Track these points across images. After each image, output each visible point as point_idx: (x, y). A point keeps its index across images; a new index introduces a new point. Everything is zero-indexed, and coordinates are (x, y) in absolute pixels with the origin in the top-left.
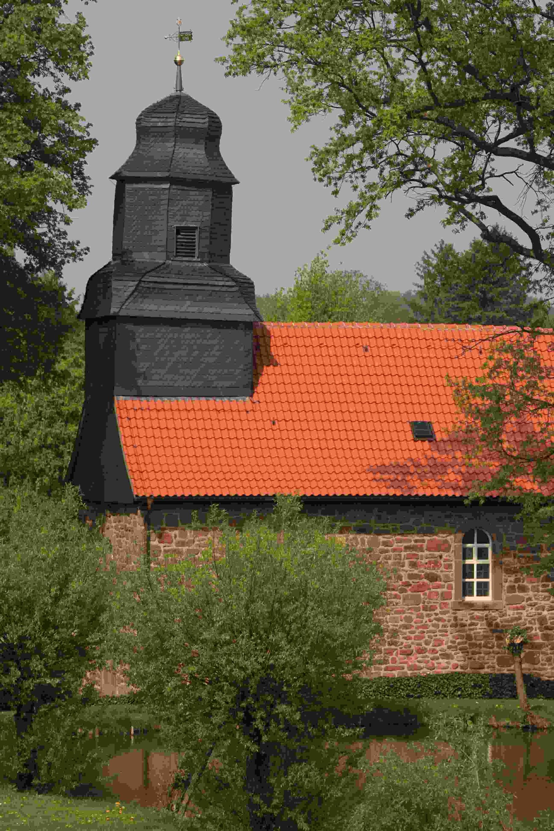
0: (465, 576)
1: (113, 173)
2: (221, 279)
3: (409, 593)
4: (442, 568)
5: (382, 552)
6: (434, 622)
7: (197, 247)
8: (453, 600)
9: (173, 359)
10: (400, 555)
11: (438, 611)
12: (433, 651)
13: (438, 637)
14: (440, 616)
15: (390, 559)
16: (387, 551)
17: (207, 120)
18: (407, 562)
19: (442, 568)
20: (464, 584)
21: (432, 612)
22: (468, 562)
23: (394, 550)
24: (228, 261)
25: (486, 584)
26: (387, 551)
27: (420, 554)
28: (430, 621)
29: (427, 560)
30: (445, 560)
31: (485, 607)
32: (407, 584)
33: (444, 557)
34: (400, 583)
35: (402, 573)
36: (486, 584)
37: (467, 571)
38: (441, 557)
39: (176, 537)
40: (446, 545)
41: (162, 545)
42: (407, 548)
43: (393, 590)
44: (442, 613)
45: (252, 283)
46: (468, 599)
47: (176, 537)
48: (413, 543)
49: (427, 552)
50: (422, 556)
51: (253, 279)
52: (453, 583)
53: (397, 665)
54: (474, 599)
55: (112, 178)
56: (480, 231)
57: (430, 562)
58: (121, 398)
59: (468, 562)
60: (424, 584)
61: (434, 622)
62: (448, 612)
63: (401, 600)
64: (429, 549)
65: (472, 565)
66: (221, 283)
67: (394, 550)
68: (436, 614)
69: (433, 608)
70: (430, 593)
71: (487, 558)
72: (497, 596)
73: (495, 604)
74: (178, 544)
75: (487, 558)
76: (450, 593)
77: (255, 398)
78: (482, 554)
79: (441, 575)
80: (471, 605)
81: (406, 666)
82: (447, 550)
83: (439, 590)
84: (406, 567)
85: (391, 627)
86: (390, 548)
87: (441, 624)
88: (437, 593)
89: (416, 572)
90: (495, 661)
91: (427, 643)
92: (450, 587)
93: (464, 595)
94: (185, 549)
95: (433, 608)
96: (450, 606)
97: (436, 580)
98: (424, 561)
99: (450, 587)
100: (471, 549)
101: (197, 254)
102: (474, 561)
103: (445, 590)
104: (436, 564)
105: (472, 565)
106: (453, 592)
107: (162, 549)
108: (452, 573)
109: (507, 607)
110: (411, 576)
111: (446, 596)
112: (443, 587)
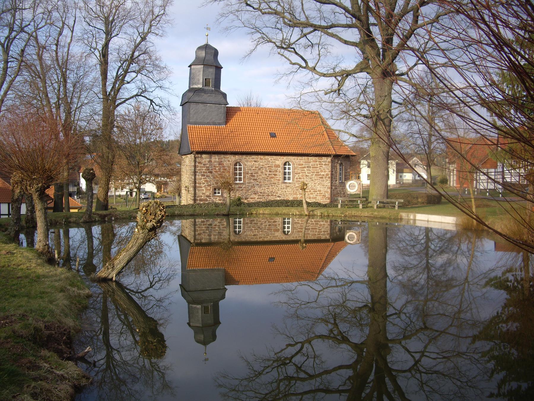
72: (293, 180)
80: (286, 183)
102: (287, 171)
104: (276, 171)
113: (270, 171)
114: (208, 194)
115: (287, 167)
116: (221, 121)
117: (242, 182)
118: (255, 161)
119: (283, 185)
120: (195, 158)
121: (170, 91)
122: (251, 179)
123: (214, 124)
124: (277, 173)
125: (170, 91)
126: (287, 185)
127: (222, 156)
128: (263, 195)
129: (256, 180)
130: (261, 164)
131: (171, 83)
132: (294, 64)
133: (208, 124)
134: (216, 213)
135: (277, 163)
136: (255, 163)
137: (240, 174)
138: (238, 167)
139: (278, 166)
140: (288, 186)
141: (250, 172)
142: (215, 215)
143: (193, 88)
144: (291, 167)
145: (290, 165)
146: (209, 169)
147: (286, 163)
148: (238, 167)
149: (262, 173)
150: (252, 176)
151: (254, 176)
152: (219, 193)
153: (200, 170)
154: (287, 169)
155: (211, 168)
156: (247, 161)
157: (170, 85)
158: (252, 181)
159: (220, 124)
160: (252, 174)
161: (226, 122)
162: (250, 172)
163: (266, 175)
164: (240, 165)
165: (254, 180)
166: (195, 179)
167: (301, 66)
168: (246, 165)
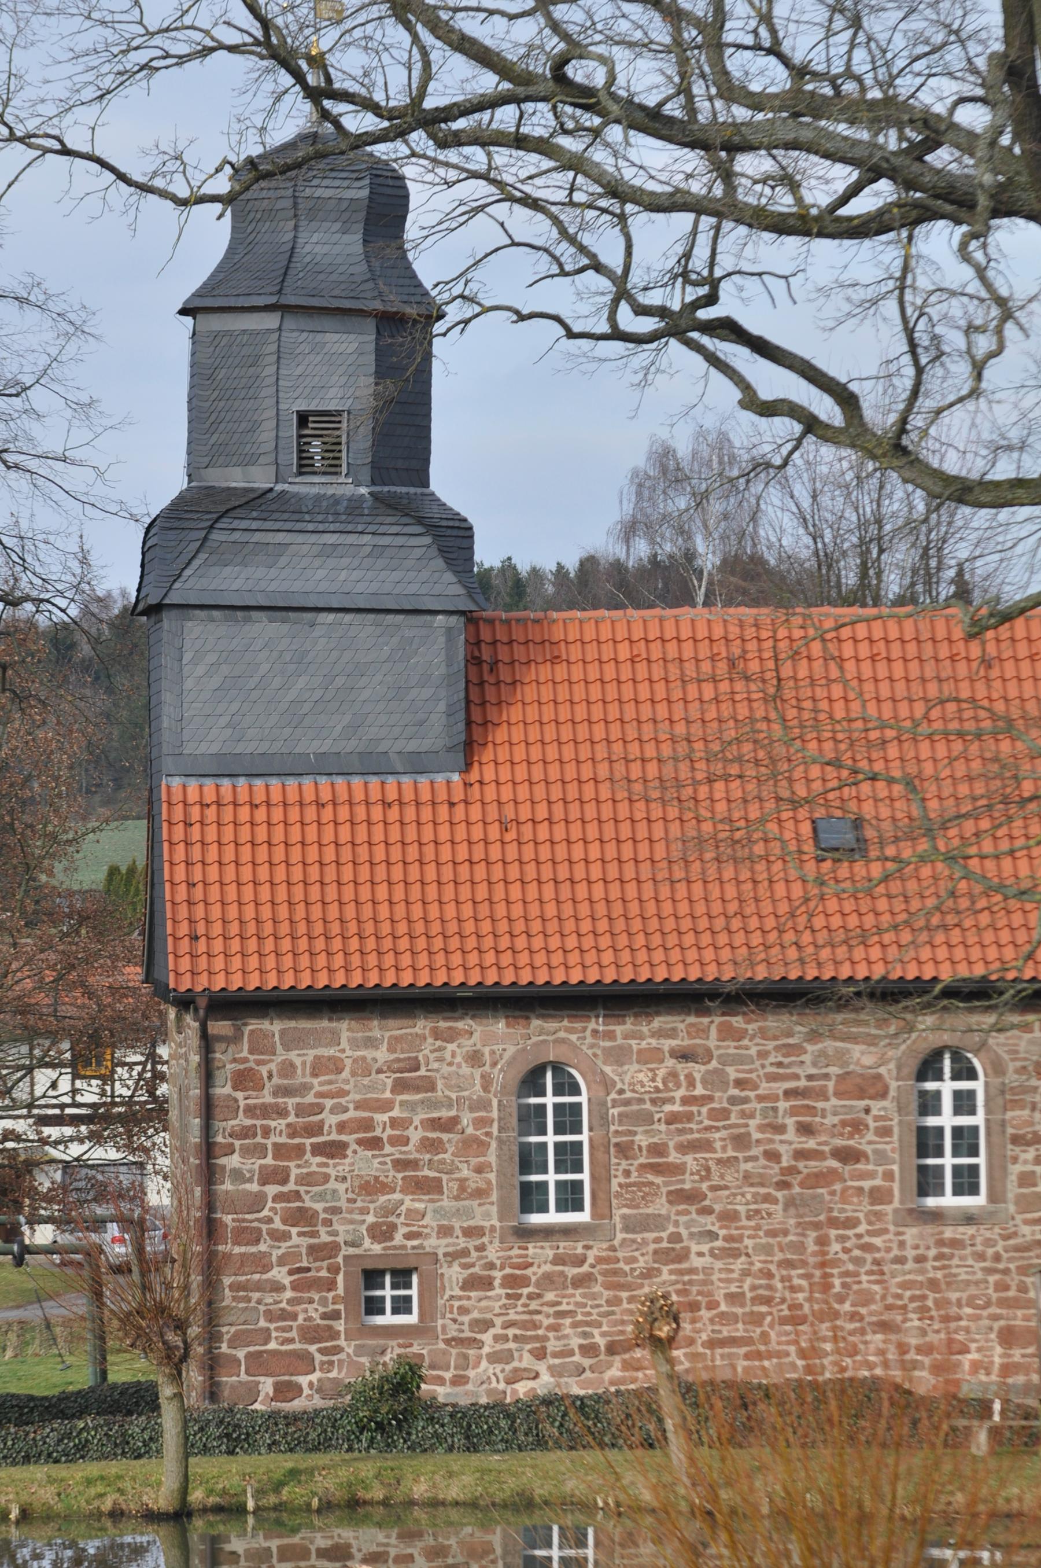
0: (923, 1150)
1: (180, 306)
2: (389, 520)
3: (797, 1190)
4: (870, 1136)
5: (733, 1101)
6: (857, 1253)
7: (344, 454)
8: (896, 1204)
9: (292, 695)
10: (775, 1109)
11: (862, 1229)
12: (854, 1316)
13: (865, 1285)
14: (867, 1239)
15: (752, 1116)
16: (746, 1100)
17: (367, 181)
18: (790, 1122)
19: (870, 1136)
20: (922, 1169)
21: (850, 1233)
22: (932, 1121)
23: (761, 1098)
24: (424, 481)
25: (974, 1169)
26: (746, 1100)
27: (820, 1105)
28: (846, 1251)
29: (836, 1120)
30: (877, 1119)
31: (969, 1218)
32: (792, 1171)
33: (874, 1112)
34: (776, 1169)
35: (782, 1149)
36: (974, 1169)
37: (927, 1142)
38: (867, 1111)
39: (270, 1077)
40: (879, 1085)
41: (240, 1095)
42: (788, 1094)
43: (762, 1185)
44: (869, 1233)
45: (471, 528)
46: (931, 1202)
47: (270, 1077)
48: (803, 1083)
49: (834, 1101)
50: (823, 1110)
51: (471, 520)
52: (895, 1168)
53: (774, 1346)
54: (948, 1200)
55: (184, 312)
56: (738, 395)
57: (844, 1123)
58: (176, 782)
59: (932, 1121)
60: (833, 1171)
61: (857, 1253)
62: (886, 1231)
63: (779, 1207)
64: (838, 1095)
65: (940, 1130)
66: (395, 529)
67: (761, 1098)
68: (859, 1236)
69: (851, 1223)
70: (844, 1190)
71: (580, 1132)
72: (993, 1197)
73: (992, 1214)
74: (277, 1092)
75: (580, 1132)
76: (890, 1191)
77: (474, 776)
78: (964, 1103)
79: (868, 1149)
80: (937, 1216)
81: (792, 1349)
82: (883, 1095)
83: (867, 1184)
84: (791, 1135)
85: (758, 1265)
86: (752, 1094)
87: (869, 1257)
88: (861, 1189)
89: (811, 1144)
90: (993, 1336)
91: (841, 1299)
92: (889, 1176)
93: (923, 1191)
94: (291, 1102)
95: (851, 1223)
96: (890, 1217)
97: (858, 1161)
98: (830, 1120)
99: (889, 1176)
100: (938, 1094)
101: (344, 469)
102: (946, 1120)
103: (878, 1182)
104: (857, 1127)
105: (940, 1130)
106: (896, 1187)
107: (242, 1103)
108: (891, 1146)
109: (1019, 1218)
110: (801, 1154)
111: (878, 1196)
112: (872, 1175)
113: (805, 1129)
114: (314, 1312)
115: (947, 1088)
116: (426, 745)
117: (583, 1217)
118: (684, 1056)
119: (911, 1234)
120: (207, 1043)
121: (75, 478)
122: (649, 1193)
123: (374, 765)
124: (866, 1142)
125: (75, 478)
126: (949, 1233)
127: (422, 1026)
128: (756, 1319)
129: (691, 1197)
130: (732, 1073)
131: (84, 408)
132: (768, 409)
133: (325, 766)
134: (107, 1505)
135: (862, 1057)
136: (683, 1068)
137: (569, 1157)
138: (550, 1100)
139: (870, 1087)
140: (955, 1243)
141: (642, 1140)
142: (99, 1515)
143: (210, 492)
144: (978, 1086)
145: (971, 1074)
146: (316, 1129)
147: (937, 1055)
148: (550, 1100)
149: (741, 1141)
150: (657, 1169)
151: (678, 1169)
152: (402, 1306)
153: (247, 1133)
154: (947, 1103)
155: (331, 1120)
156: (619, 1056)
157: (80, 435)
158: (660, 1206)
159: (418, 765)
160: (657, 1150)
161: (469, 749)
162: (642, 1140)
163: (773, 1156)
164: (567, 1086)
165: (680, 1197)
166: (210, 1204)
167: (811, 424)
168: (607, 1085)
